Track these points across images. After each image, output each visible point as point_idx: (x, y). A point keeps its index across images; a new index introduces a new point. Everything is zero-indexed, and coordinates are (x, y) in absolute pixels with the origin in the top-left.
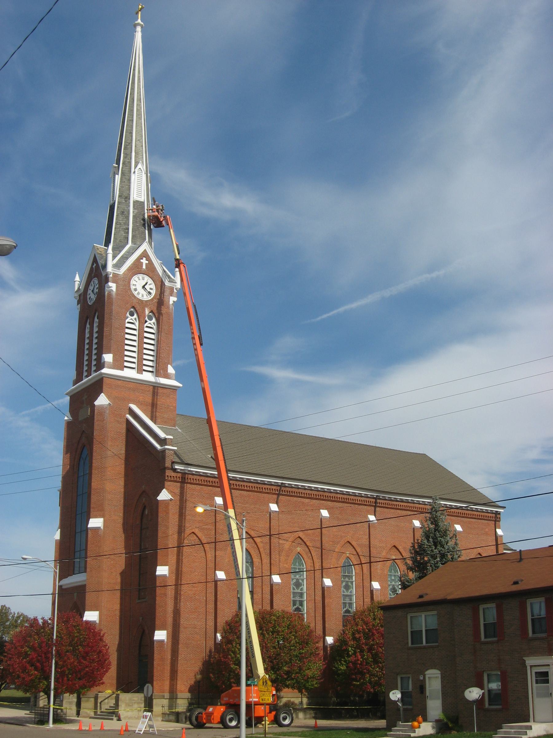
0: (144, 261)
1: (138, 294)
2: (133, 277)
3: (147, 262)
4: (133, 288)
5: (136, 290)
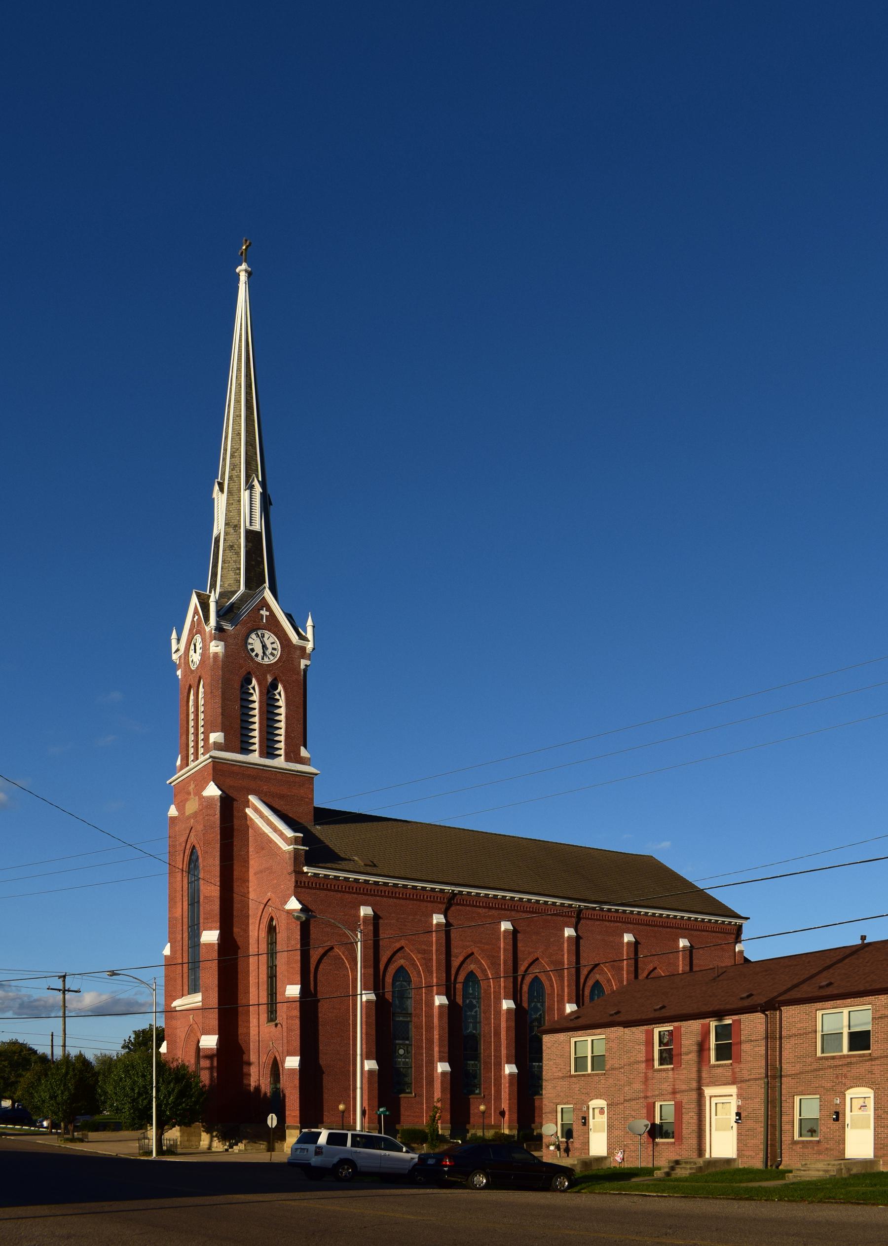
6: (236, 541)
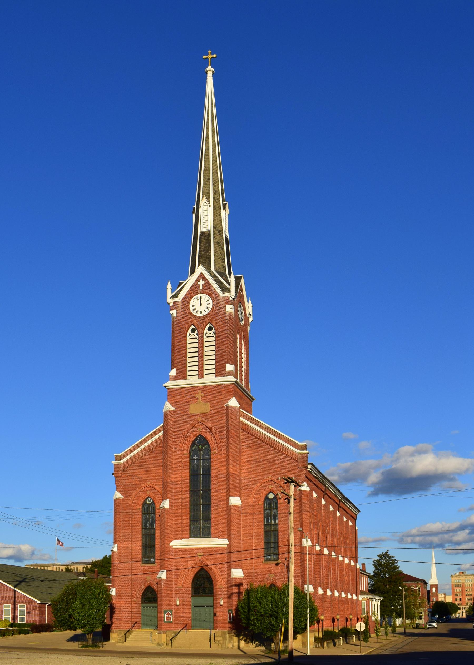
3: (204, 282)
4: (208, 311)
5: (194, 309)
6: (221, 240)
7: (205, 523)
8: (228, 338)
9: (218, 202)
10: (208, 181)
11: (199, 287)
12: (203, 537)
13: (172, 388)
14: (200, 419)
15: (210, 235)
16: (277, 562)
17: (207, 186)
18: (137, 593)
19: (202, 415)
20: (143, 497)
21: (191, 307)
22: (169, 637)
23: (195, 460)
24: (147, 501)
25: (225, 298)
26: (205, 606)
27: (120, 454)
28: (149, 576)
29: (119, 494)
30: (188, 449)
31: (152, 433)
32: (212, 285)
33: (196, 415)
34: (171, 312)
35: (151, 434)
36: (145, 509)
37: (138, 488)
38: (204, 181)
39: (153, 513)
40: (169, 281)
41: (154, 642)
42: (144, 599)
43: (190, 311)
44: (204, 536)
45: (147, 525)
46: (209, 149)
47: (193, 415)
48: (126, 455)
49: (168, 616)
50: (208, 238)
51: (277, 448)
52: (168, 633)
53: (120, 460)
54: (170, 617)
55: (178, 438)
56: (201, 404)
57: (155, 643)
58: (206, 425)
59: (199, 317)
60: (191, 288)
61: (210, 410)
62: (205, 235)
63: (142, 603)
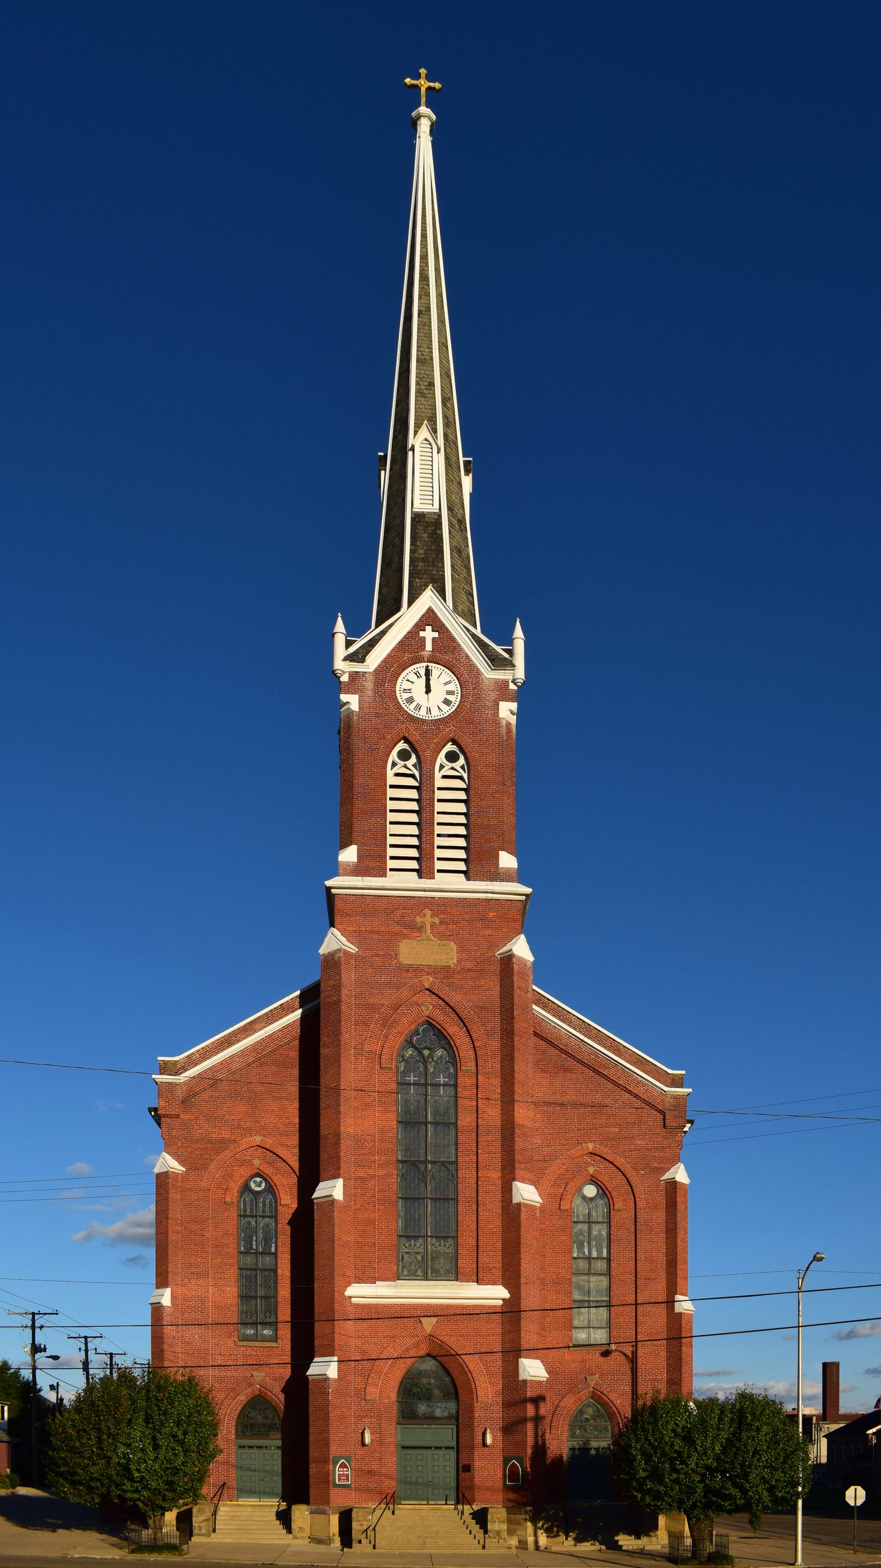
0: (429, 634)
1: (418, 707)
2: (462, 696)
3: (436, 635)
4: (447, 710)
5: (410, 700)
7: (440, 1245)
8: (504, 784)
9: (454, 450)
10: (430, 390)
11: (425, 646)
12: (433, 1278)
13: (349, 895)
14: (428, 981)
15: (441, 524)
16: (605, 1349)
17: (428, 401)
18: (226, 1413)
19: (433, 970)
20: (242, 1173)
21: (402, 692)
22: (359, 1523)
23: (409, 1084)
24: (252, 1185)
25: (497, 681)
26: (431, 1448)
27: (177, 1058)
28: (259, 1372)
29: (173, 1160)
30: (392, 1056)
31: (267, 1013)
32: (459, 645)
33: (417, 970)
34: (344, 698)
35: (264, 1015)
36: (245, 1204)
37: (226, 1148)
38: (418, 386)
39: (268, 1214)
40: (339, 614)
41: (300, 1535)
42: (242, 1428)
43: (399, 703)
44: (435, 1276)
45: (251, 1245)
46: (428, 309)
47: (408, 971)
48: (192, 1062)
49: (342, 1469)
50: (435, 530)
51: (612, 1078)
52: (357, 1512)
53: (177, 1073)
54: (348, 1473)
55: (365, 1024)
56: (431, 942)
57: (303, 1538)
58: (446, 999)
59: (423, 721)
60: (401, 644)
61: (455, 961)
62: (426, 522)
63: (238, 1437)
